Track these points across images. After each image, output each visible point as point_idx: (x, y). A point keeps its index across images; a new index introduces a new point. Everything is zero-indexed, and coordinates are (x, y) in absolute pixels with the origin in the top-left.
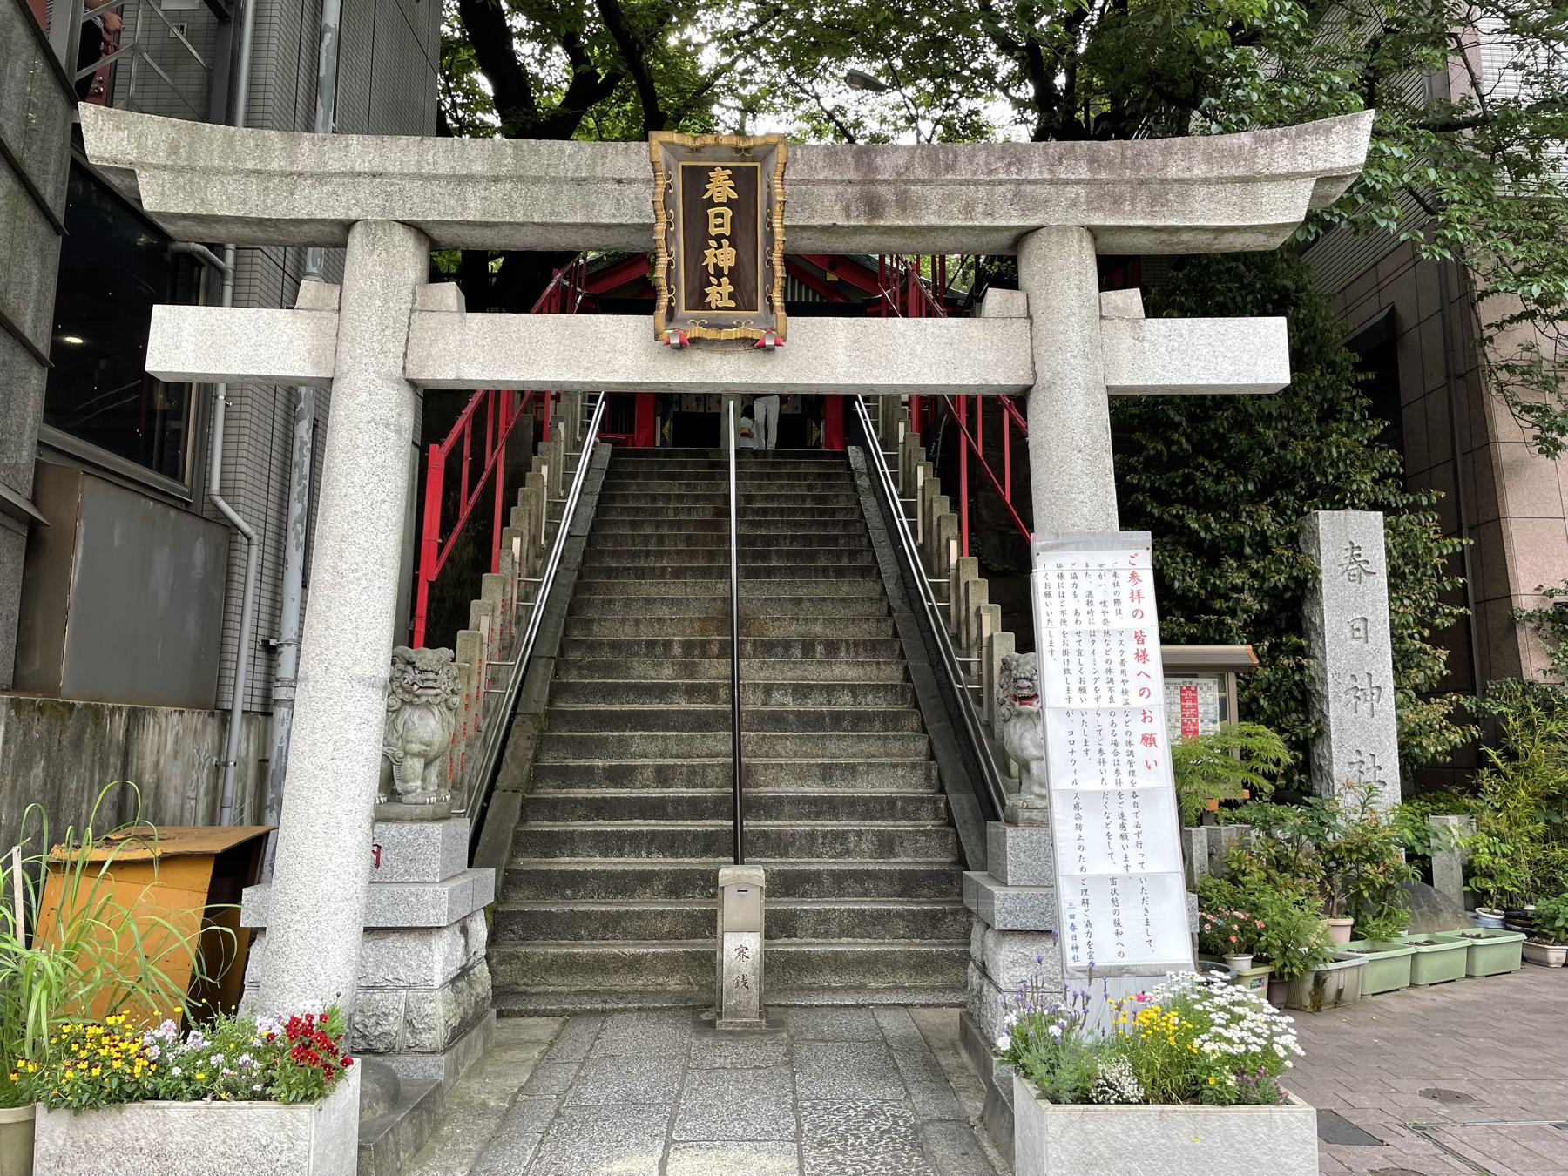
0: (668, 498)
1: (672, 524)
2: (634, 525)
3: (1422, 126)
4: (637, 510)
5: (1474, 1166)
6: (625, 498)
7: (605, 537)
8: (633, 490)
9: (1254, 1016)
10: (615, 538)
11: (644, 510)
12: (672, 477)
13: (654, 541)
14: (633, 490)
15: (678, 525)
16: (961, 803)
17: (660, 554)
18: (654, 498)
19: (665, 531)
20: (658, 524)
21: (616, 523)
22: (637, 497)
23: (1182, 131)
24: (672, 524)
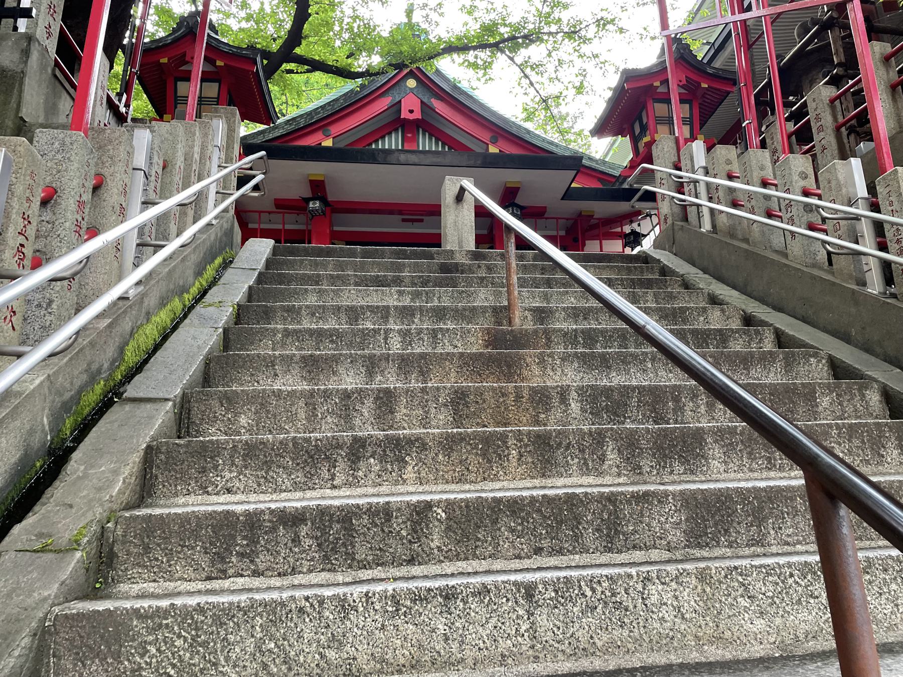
0: (384, 313)
1: (405, 364)
2: (313, 366)
3: (760, 126)
4: (319, 335)
5: (47, 468)
6: (293, 313)
7: (230, 400)
8: (312, 300)
9: (528, 639)
10: (261, 401)
11: (333, 336)
12: (380, 282)
13: (367, 409)
14: (312, 300)
15: (419, 365)
16: (135, 330)
17: (396, 451)
18: (354, 314)
19: (391, 380)
20: (372, 366)
21: (270, 363)
22: (313, 312)
23: (367, 26)
24: (405, 364)
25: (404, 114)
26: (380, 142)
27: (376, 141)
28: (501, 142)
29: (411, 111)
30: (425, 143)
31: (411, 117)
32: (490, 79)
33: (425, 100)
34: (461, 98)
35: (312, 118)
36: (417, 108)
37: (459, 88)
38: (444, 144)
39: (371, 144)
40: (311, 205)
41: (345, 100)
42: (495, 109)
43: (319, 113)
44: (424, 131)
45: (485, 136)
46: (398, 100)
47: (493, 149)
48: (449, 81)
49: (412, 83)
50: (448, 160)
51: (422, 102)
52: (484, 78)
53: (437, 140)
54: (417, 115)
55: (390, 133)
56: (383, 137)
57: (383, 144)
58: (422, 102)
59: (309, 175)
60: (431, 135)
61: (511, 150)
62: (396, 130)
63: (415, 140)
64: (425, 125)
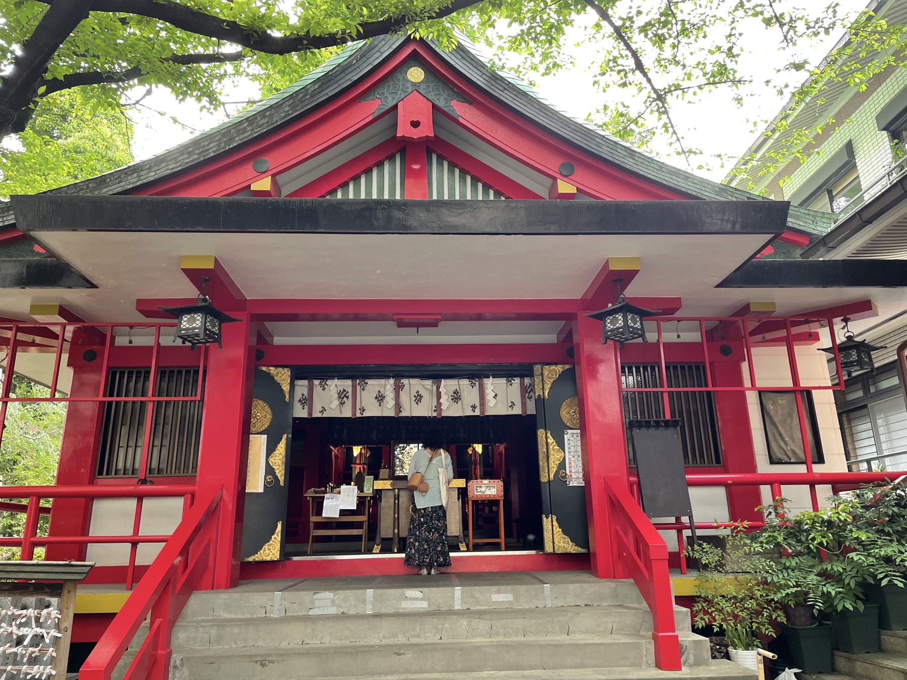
25: (404, 130)
26: (351, 187)
27: (344, 185)
28: (580, 174)
29: (415, 124)
30: (444, 184)
31: (415, 133)
32: (555, 65)
33: (441, 104)
34: (506, 97)
35: (232, 140)
36: (426, 118)
37: (502, 79)
38: (487, 187)
39: (334, 191)
40: (609, 326)
41: (293, 107)
42: (557, 109)
43: (244, 130)
44: (441, 158)
45: (552, 163)
46: (391, 104)
47: (564, 187)
48: (483, 65)
49: (416, 74)
50: (484, 218)
51: (435, 107)
52: (544, 65)
53: (475, 180)
54: (426, 131)
55: (380, 164)
56: (356, 178)
57: (357, 190)
58: (435, 107)
59: (182, 258)
60: (452, 166)
61: (611, 194)
62: (391, 158)
63: (424, 174)
64: (433, 148)
